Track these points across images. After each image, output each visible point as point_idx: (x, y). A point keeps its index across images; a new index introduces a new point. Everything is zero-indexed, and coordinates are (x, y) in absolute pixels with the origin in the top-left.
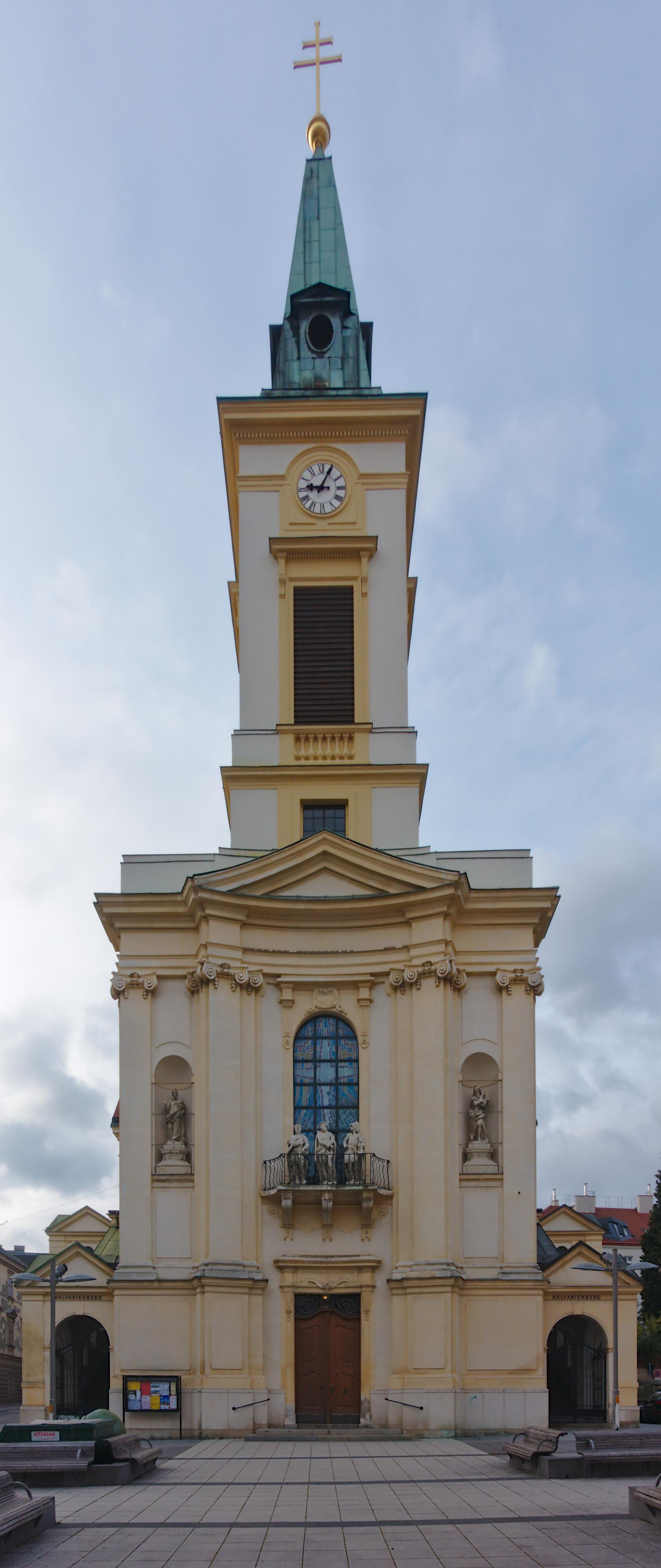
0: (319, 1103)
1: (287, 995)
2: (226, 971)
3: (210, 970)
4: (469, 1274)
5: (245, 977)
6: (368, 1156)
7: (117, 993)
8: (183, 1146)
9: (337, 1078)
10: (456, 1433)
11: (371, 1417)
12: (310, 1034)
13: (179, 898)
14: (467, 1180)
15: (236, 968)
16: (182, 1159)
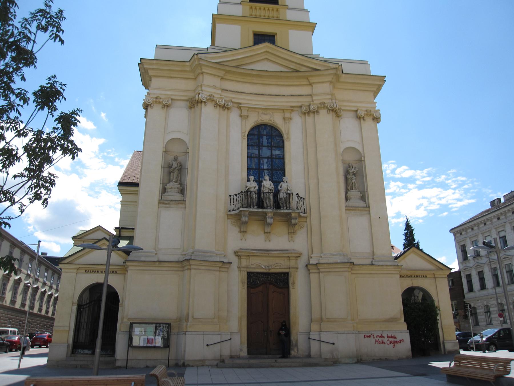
0: (262, 167)
1: (245, 113)
3: (204, 96)
4: (356, 262)
5: (223, 103)
7: (146, 106)
9: (272, 155)
10: (357, 360)
11: (298, 350)
12: (256, 133)
13: (188, 64)
14: (349, 210)
15: (217, 98)
16: (178, 192)
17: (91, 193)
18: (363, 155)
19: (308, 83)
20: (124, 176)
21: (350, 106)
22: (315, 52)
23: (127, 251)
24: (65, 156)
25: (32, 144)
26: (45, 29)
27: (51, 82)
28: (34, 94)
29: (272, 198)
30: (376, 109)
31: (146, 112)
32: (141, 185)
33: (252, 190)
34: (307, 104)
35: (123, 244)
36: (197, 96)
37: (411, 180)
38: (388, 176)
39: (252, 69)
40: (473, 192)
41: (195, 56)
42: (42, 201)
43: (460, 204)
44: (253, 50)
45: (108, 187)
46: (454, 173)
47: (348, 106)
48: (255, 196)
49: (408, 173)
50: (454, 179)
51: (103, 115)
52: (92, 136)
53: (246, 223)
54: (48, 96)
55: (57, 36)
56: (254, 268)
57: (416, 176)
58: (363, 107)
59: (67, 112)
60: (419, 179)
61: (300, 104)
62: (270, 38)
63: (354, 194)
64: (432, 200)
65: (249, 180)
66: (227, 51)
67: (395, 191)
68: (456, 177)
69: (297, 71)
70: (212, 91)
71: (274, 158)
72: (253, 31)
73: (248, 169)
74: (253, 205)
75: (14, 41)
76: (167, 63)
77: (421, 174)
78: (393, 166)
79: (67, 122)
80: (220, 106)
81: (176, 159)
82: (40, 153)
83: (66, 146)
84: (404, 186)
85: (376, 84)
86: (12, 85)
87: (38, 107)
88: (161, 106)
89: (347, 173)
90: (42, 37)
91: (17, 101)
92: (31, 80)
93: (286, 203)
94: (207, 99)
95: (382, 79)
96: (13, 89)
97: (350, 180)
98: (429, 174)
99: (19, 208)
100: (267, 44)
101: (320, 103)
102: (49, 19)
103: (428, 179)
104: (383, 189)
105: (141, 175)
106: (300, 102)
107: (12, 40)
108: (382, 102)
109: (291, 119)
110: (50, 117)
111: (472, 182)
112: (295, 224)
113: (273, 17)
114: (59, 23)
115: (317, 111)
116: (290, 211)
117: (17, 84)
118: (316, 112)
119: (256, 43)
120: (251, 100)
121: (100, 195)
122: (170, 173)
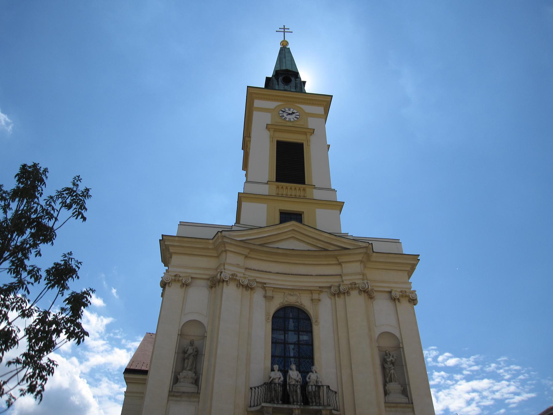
1: (269, 294)
3: (226, 275)
5: (246, 283)
6: (325, 387)
7: (164, 285)
8: (194, 374)
9: (299, 340)
13: (211, 241)
15: (241, 277)
16: (192, 383)
17: (91, 380)
18: (401, 341)
19: (337, 262)
20: (132, 361)
21: (383, 287)
22: (344, 230)
24: (69, 340)
25: (36, 325)
26: (69, 207)
27: (66, 258)
28: (48, 271)
29: (299, 391)
31: (164, 290)
32: (150, 374)
33: (276, 381)
34: (337, 284)
36: (219, 275)
37: (457, 369)
38: (429, 365)
39: (278, 248)
40: (531, 384)
41: (219, 234)
42: (35, 393)
43: (517, 399)
44: (279, 228)
45: (110, 373)
46: (505, 361)
47: (380, 287)
48: (280, 389)
49: (452, 362)
50: (506, 368)
51: (114, 291)
52: (99, 315)
54: (61, 274)
55: (80, 213)
57: (462, 364)
59: (79, 292)
60: (465, 369)
61: (328, 285)
62: (297, 217)
63: (393, 386)
64: (485, 393)
65: (272, 370)
66: (252, 229)
67: (440, 382)
68: (508, 365)
69: (325, 250)
70: (235, 269)
72: (280, 210)
73: (272, 356)
74: (277, 399)
75: (37, 218)
76: (190, 240)
77: (468, 363)
78: (434, 353)
79: (78, 302)
80: (243, 286)
81: (192, 344)
82: (42, 338)
83: (72, 329)
85: (410, 263)
86: (26, 262)
87: (49, 285)
88: (179, 284)
89: (384, 362)
90: (65, 214)
91: (28, 278)
92: (46, 257)
93: (315, 398)
94: (230, 279)
95: (415, 258)
96: (25, 265)
97: (388, 371)
98: (477, 363)
99: (7, 401)
100: (293, 222)
101: (351, 284)
102: (75, 197)
103: (475, 368)
105: (151, 361)
107: (33, 216)
108: (418, 282)
109: (319, 300)
110: (60, 295)
111: (528, 372)
113: (300, 196)
115: (348, 292)
116: (321, 408)
117: (32, 261)
118: (347, 293)
119: (282, 221)
120: (277, 280)
121: (101, 383)
122: (184, 360)
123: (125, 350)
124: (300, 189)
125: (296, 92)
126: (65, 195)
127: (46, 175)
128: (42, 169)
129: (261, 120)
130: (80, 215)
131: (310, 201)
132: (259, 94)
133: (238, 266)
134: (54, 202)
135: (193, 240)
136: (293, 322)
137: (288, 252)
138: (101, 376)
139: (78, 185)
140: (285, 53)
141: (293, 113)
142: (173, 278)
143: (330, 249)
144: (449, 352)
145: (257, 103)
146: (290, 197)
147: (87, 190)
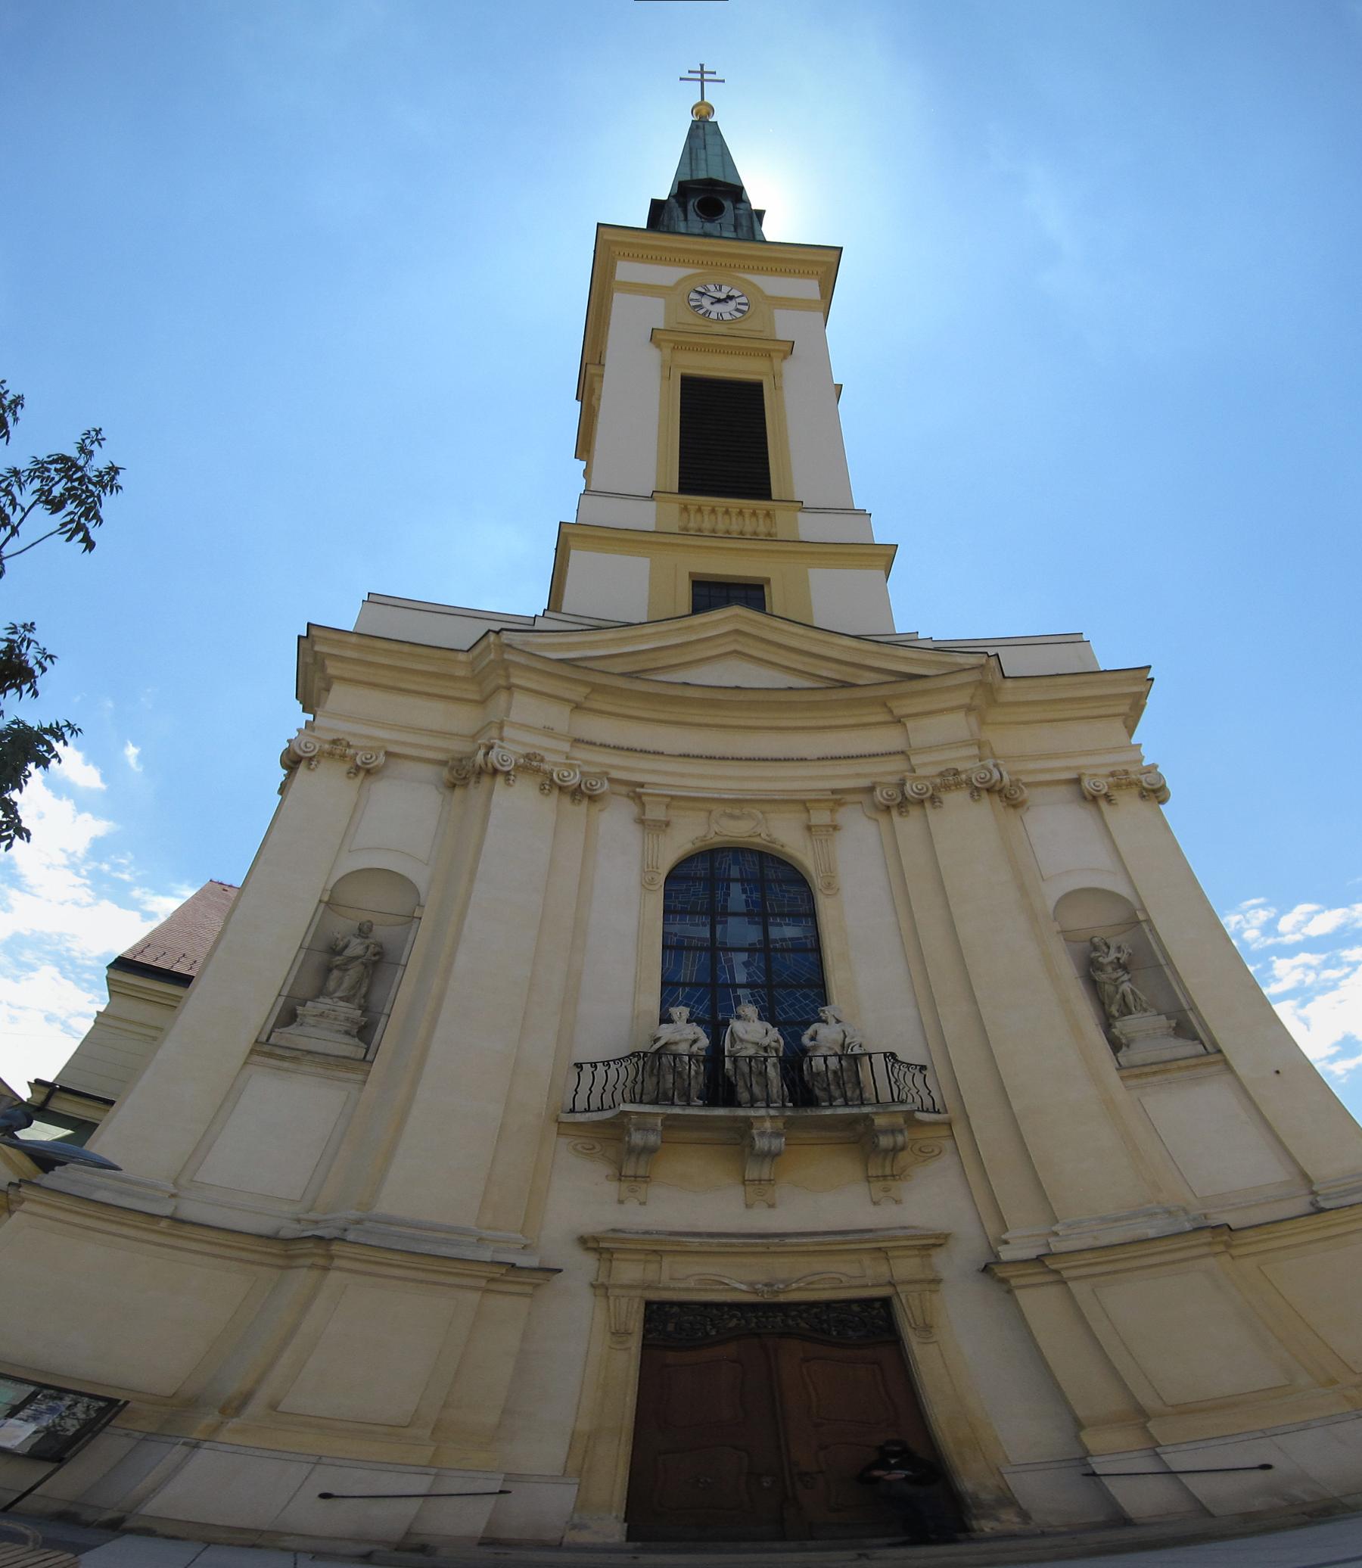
1: (655, 813)
2: (535, 764)
3: (507, 754)
4: (1233, 1219)
5: (573, 780)
7: (292, 761)
13: (462, 657)
15: (555, 764)
16: (347, 1033)
18: (1137, 905)
22: (902, 624)
23: (44, 1158)
26: (56, 505)
29: (773, 1073)
30: (1144, 764)
31: (288, 777)
33: (683, 1048)
34: (894, 779)
35: (42, 1132)
41: (492, 637)
45: (72, 961)
49: (1327, 922)
51: (132, 751)
53: (649, 1151)
55: (80, 527)
56: (687, 1290)
58: (1097, 771)
62: (750, 594)
65: (665, 1019)
69: (846, 685)
71: (775, 950)
72: (691, 574)
78: (1263, 915)
80: (561, 788)
84: (1329, 959)
85: (1130, 691)
88: (346, 767)
89: (1091, 972)
90: (41, 521)
94: (517, 767)
97: (1109, 988)
101: (941, 774)
102: (76, 484)
104: (1253, 988)
106: (865, 776)
108: (1155, 740)
112: (896, 1150)
114: (99, 497)
115: (932, 798)
116: (866, 1110)
119: (697, 608)
120: (682, 775)
123: (136, 915)
124: (754, 514)
125: (738, 239)
126: (53, 474)
127: (15, 413)
128: (10, 397)
129: (635, 318)
130: (79, 531)
131: (790, 547)
132: (631, 245)
133: (548, 731)
134: (21, 485)
135: (406, 648)
136: (744, 891)
137: (719, 695)
138: (39, 959)
139: (91, 453)
140: (703, 134)
141: (730, 298)
142: (327, 747)
143: (860, 682)
144: (1309, 901)
145: (626, 271)
146: (725, 536)
147: (114, 470)
